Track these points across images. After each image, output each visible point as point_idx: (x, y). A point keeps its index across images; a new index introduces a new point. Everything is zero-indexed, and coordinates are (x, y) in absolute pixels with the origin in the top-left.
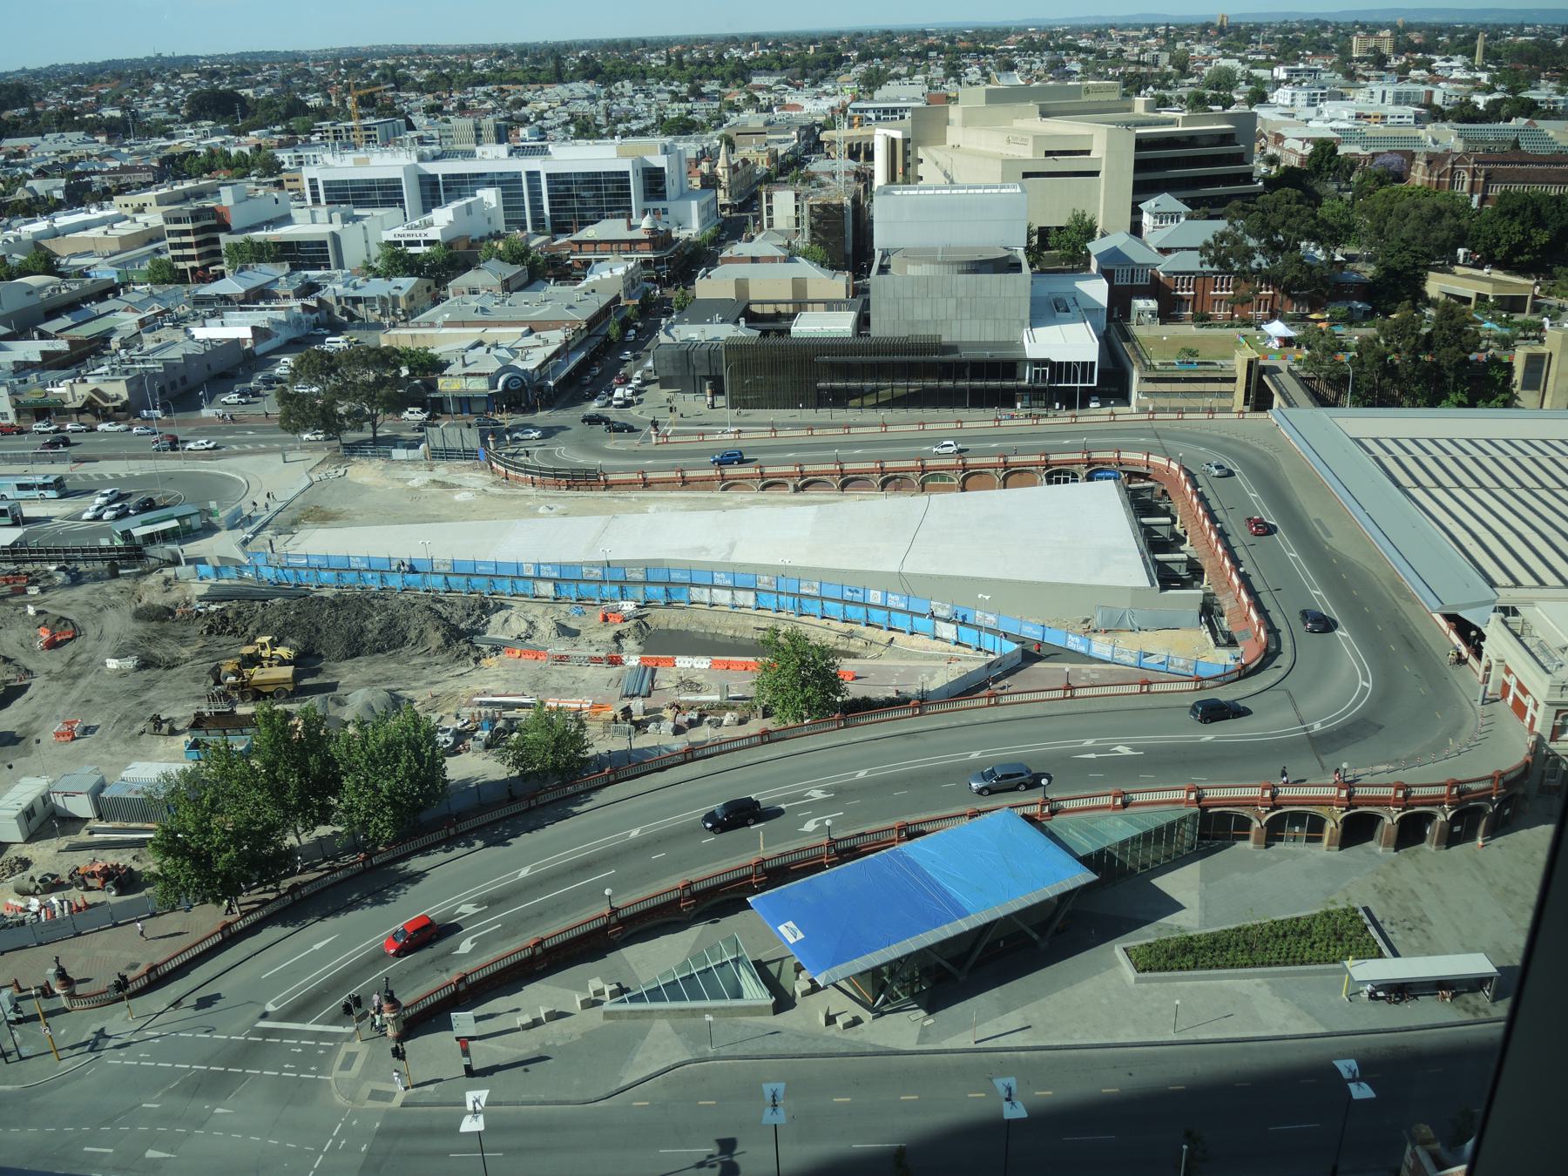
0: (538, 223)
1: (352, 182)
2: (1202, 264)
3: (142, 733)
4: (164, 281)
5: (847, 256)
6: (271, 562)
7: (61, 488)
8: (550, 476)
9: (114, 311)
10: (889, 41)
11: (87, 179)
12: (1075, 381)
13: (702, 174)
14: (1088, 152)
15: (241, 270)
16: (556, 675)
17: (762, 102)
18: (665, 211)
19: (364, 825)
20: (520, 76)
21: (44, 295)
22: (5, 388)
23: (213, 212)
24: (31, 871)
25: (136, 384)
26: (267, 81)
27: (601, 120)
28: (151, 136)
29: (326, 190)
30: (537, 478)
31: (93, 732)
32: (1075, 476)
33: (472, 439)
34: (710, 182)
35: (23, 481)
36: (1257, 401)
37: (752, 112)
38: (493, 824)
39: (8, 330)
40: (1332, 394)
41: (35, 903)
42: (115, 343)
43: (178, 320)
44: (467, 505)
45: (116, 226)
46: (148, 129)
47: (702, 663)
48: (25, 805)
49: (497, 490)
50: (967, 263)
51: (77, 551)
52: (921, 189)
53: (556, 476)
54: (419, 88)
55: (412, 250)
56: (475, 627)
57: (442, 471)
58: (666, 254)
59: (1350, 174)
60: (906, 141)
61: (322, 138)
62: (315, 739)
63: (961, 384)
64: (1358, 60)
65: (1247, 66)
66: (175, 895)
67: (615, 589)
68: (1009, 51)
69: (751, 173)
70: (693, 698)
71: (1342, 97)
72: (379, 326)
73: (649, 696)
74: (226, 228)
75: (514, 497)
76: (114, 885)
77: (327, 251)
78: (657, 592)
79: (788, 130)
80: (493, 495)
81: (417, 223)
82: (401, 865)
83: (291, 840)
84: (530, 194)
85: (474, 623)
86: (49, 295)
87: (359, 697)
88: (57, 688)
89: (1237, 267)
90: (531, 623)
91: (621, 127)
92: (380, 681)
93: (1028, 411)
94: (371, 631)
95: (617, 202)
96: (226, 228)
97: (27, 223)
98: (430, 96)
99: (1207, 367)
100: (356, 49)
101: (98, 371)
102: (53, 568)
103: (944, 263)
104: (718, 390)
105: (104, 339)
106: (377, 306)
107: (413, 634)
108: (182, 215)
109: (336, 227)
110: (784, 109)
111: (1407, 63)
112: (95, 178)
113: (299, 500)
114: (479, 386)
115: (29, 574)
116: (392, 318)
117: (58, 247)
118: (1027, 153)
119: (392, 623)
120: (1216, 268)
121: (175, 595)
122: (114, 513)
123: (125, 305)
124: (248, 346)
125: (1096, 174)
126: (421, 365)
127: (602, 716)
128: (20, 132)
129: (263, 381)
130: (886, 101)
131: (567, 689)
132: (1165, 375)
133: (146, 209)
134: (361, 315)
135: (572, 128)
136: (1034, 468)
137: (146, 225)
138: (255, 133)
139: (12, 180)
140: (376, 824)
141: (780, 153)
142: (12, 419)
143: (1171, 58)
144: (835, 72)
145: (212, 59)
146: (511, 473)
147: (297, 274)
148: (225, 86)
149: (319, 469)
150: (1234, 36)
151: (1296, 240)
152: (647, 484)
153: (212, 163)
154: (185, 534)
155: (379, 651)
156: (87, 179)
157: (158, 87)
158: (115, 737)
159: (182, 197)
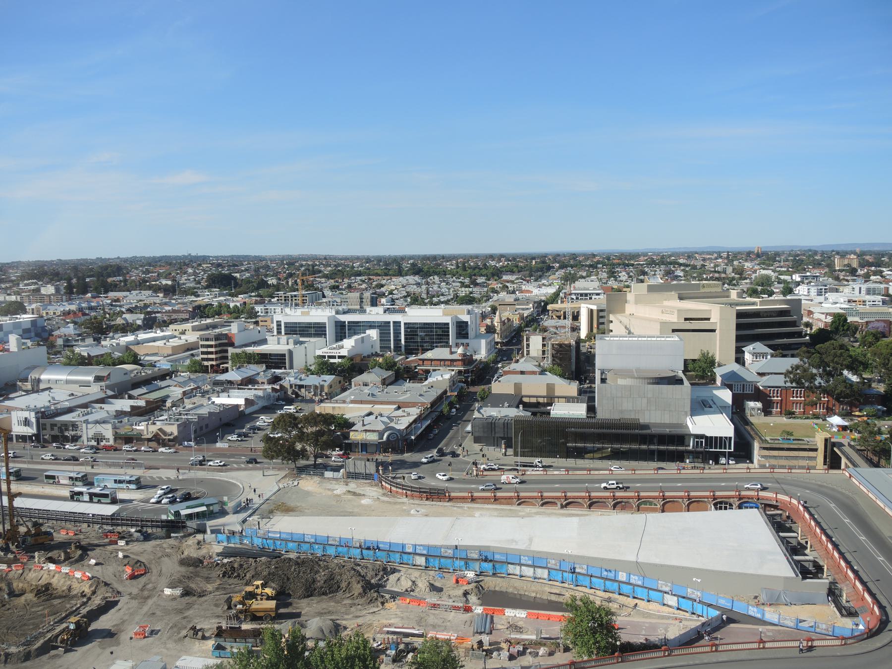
0: (397, 348)
2: (785, 382)
3: (185, 637)
4: (196, 371)
5: (572, 372)
7: (139, 484)
8: (417, 492)
9: (169, 386)
10: (574, 259)
12: (725, 448)
13: (487, 326)
14: (708, 319)
15: (239, 368)
16: (432, 617)
17: (510, 289)
20: (379, 272)
21: (132, 375)
22: (110, 425)
26: (246, 270)
28: (186, 295)
29: (286, 327)
30: (409, 492)
31: (156, 634)
32: (731, 505)
33: (371, 468)
34: (490, 330)
35: (118, 478)
36: (831, 462)
37: (505, 293)
39: (113, 393)
40: (875, 459)
42: (168, 404)
43: (204, 392)
44: (368, 507)
45: (170, 340)
46: (185, 291)
47: (521, 614)
50: (653, 378)
51: (149, 521)
52: (611, 337)
53: (420, 492)
54: (327, 277)
55: (332, 361)
56: (380, 582)
57: (353, 485)
59: (855, 333)
60: (599, 311)
61: (278, 300)
63: (652, 447)
64: (839, 270)
65: (776, 274)
67: (462, 563)
68: (642, 265)
69: (511, 326)
70: (518, 636)
71: (837, 291)
72: (311, 401)
73: (491, 633)
74: (232, 345)
75: (395, 503)
79: (528, 303)
80: (383, 502)
81: (335, 346)
84: (394, 333)
85: (380, 580)
86: (135, 376)
88: (134, 603)
89: (807, 384)
90: (414, 582)
91: (435, 300)
92: (325, 613)
93: (693, 465)
94: (319, 582)
96: (232, 345)
97: (122, 336)
98: (332, 281)
99: (800, 442)
102: (133, 530)
103: (639, 378)
105: (163, 400)
106: (312, 390)
107: (343, 585)
109: (291, 346)
110: (522, 292)
111: (868, 273)
112: (158, 315)
114: (373, 437)
115: (119, 533)
117: (140, 350)
118: (674, 319)
119: (331, 578)
120: (794, 385)
121: (203, 552)
122: (168, 500)
123: (176, 383)
124: (242, 409)
125: (714, 331)
126: (339, 424)
127: (464, 645)
129: (250, 429)
131: (439, 626)
132: (774, 446)
133: (186, 332)
135: (409, 300)
136: (706, 500)
137: (187, 341)
138: (242, 296)
139: (114, 314)
142: (111, 442)
143: (734, 269)
145: (217, 258)
147: (269, 371)
149: (283, 480)
150: (767, 258)
151: (841, 369)
152: (473, 499)
153: (219, 311)
154: (210, 515)
156: (154, 315)
157: (190, 270)
158: (169, 638)
159: (205, 327)
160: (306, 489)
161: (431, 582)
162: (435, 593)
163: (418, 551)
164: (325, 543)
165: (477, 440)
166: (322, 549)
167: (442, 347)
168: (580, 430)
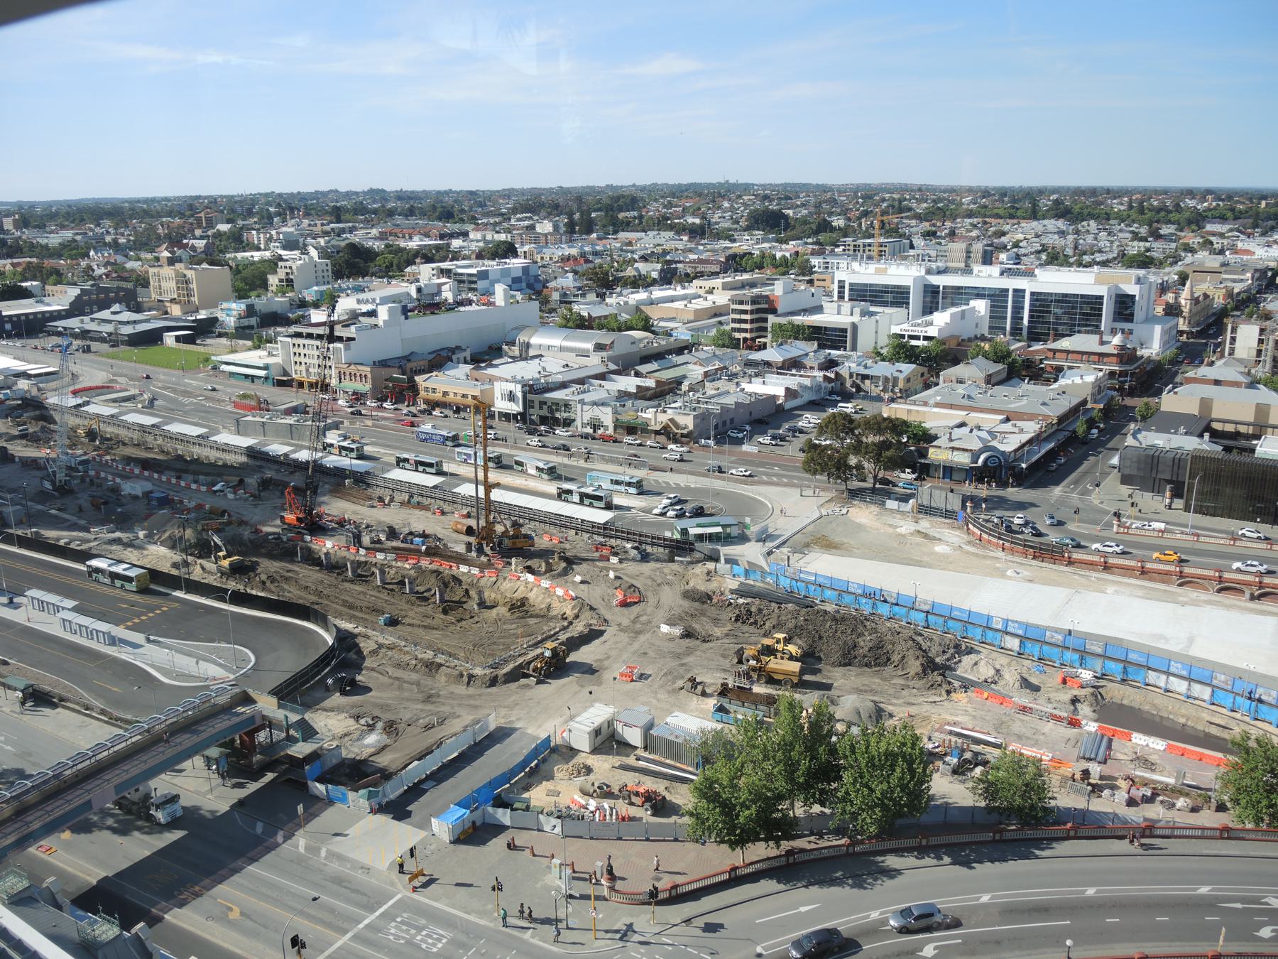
0: (1016, 331)
1: (871, 285)
3: (681, 689)
4: (724, 346)
6: (787, 574)
7: (641, 489)
9: (687, 363)
11: (674, 266)
15: (781, 344)
16: (1018, 723)
17: (1216, 246)
18: (1131, 332)
19: (854, 816)
20: (1001, 212)
21: (642, 345)
23: (767, 299)
24: (592, 777)
25: (702, 418)
26: (803, 205)
27: (1069, 252)
28: (719, 239)
30: (1007, 544)
31: (646, 679)
33: (955, 503)
34: (1173, 311)
37: (1206, 253)
38: (962, 845)
39: (616, 368)
41: (593, 804)
42: (685, 387)
43: (732, 375)
47: (1158, 744)
48: (596, 724)
49: (971, 549)
51: (648, 537)
53: (1025, 546)
54: (919, 217)
55: (914, 343)
56: (948, 663)
57: (925, 524)
58: (1130, 368)
61: (844, 250)
62: (820, 729)
66: (702, 831)
67: (1076, 656)
69: (1210, 306)
70: (1147, 775)
72: (879, 399)
73: (1105, 763)
74: (774, 311)
75: (985, 557)
77: (846, 337)
78: (1115, 668)
79: (1243, 271)
80: (968, 553)
81: (920, 321)
82: (880, 859)
84: (1013, 307)
85: (948, 660)
87: (850, 702)
88: (624, 637)
91: (1087, 258)
92: (866, 691)
95: (1087, 320)
96: (774, 311)
97: (632, 293)
98: (927, 224)
100: (869, 185)
101: (673, 405)
102: (629, 546)
104: (1177, 494)
105: (678, 381)
106: (880, 383)
108: (745, 299)
109: (856, 318)
112: (679, 266)
113: (811, 528)
114: (963, 459)
116: (891, 394)
119: (879, 646)
121: (713, 585)
124: (780, 402)
127: (1061, 771)
129: (789, 430)
131: (1028, 738)
133: (715, 291)
137: (714, 303)
138: (794, 242)
139: (624, 262)
141: (1236, 291)
142: (610, 431)
145: (764, 186)
146: (985, 536)
148: (774, 207)
149: (827, 505)
154: (726, 539)
155: (866, 665)
156: (674, 266)
157: (726, 204)
158: (662, 687)
159: (740, 285)
162: (1028, 691)
163: (1010, 629)
164: (876, 597)
165: (1126, 480)
166: (871, 605)
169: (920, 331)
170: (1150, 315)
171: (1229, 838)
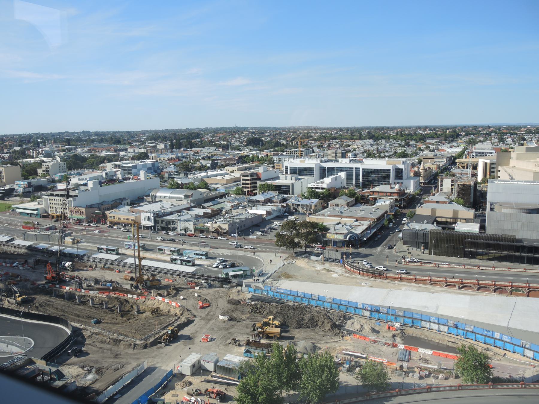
0: (357, 184)
3: (230, 343)
4: (239, 194)
6: (272, 290)
7: (207, 256)
9: (224, 202)
11: (216, 161)
15: (263, 193)
16: (372, 348)
17: (431, 148)
19: (308, 394)
20: (347, 137)
21: (205, 195)
24: (192, 387)
25: (232, 225)
26: (268, 136)
27: (375, 152)
28: (235, 150)
30: (361, 272)
31: (214, 340)
33: (339, 256)
34: (417, 174)
35: (196, 252)
37: (427, 151)
42: (224, 212)
44: (336, 279)
46: (234, 148)
47: (429, 352)
49: (346, 275)
50: (526, 209)
51: (211, 277)
52: (499, 181)
54: (315, 140)
55: (317, 190)
56: (341, 324)
57: (327, 265)
61: (286, 153)
62: (290, 357)
63: (523, 254)
67: (393, 317)
69: (431, 172)
72: (304, 214)
73: (409, 362)
74: (259, 179)
75: (352, 278)
76: (219, 398)
79: (443, 158)
80: (345, 276)
81: (319, 182)
83: (284, 394)
84: (356, 175)
85: (341, 322)
88: (203, 322)
90: (362, 326)
91: (382, 155)
96: (259, 179)
97: (200, 173)
101: (219, 220)
102: (203, 282)
103: (517, 209)
104: (426, 247)
105: (221, 210)
106: (305, 208)
109: (293, 181)
110: (439, 151)
112: (219, 161)
113: (280, 269)
114: (340, 238)
116: (309, 212)
117: (209, 181)
119: (312, 318)
121: (241, 297)
124: (264, 217)
126: (320, 228)
127: (391, 367)
128: (197, 146)
129: (269, 229)
130: (480, 150)
131: (376, 354)
133: (234, 171)
134: (299, 210)
135: (365, 154)
138: (266, 151)
139: (195, 160)
140: (312, 396)
141: (441, 165)
142: (193, 232)
144: (456, 139)
145: (252, 128)
146: (352, 269)
147: (280, 195)
148: (257, 136)
152: (401, 279)
155: (308, 327)
156: (216, 161)
157: (237, 136)
159: (245, 169)
160: (300, 265)
161: (373, 327)
162: (375, 333)
164: (310, 298)
165: (405, 243)
166: (308, 302)
167: (385, 184)
168: (474, 240)
169: (319, 186)
170: (409, 176)
171: (462, 390)
